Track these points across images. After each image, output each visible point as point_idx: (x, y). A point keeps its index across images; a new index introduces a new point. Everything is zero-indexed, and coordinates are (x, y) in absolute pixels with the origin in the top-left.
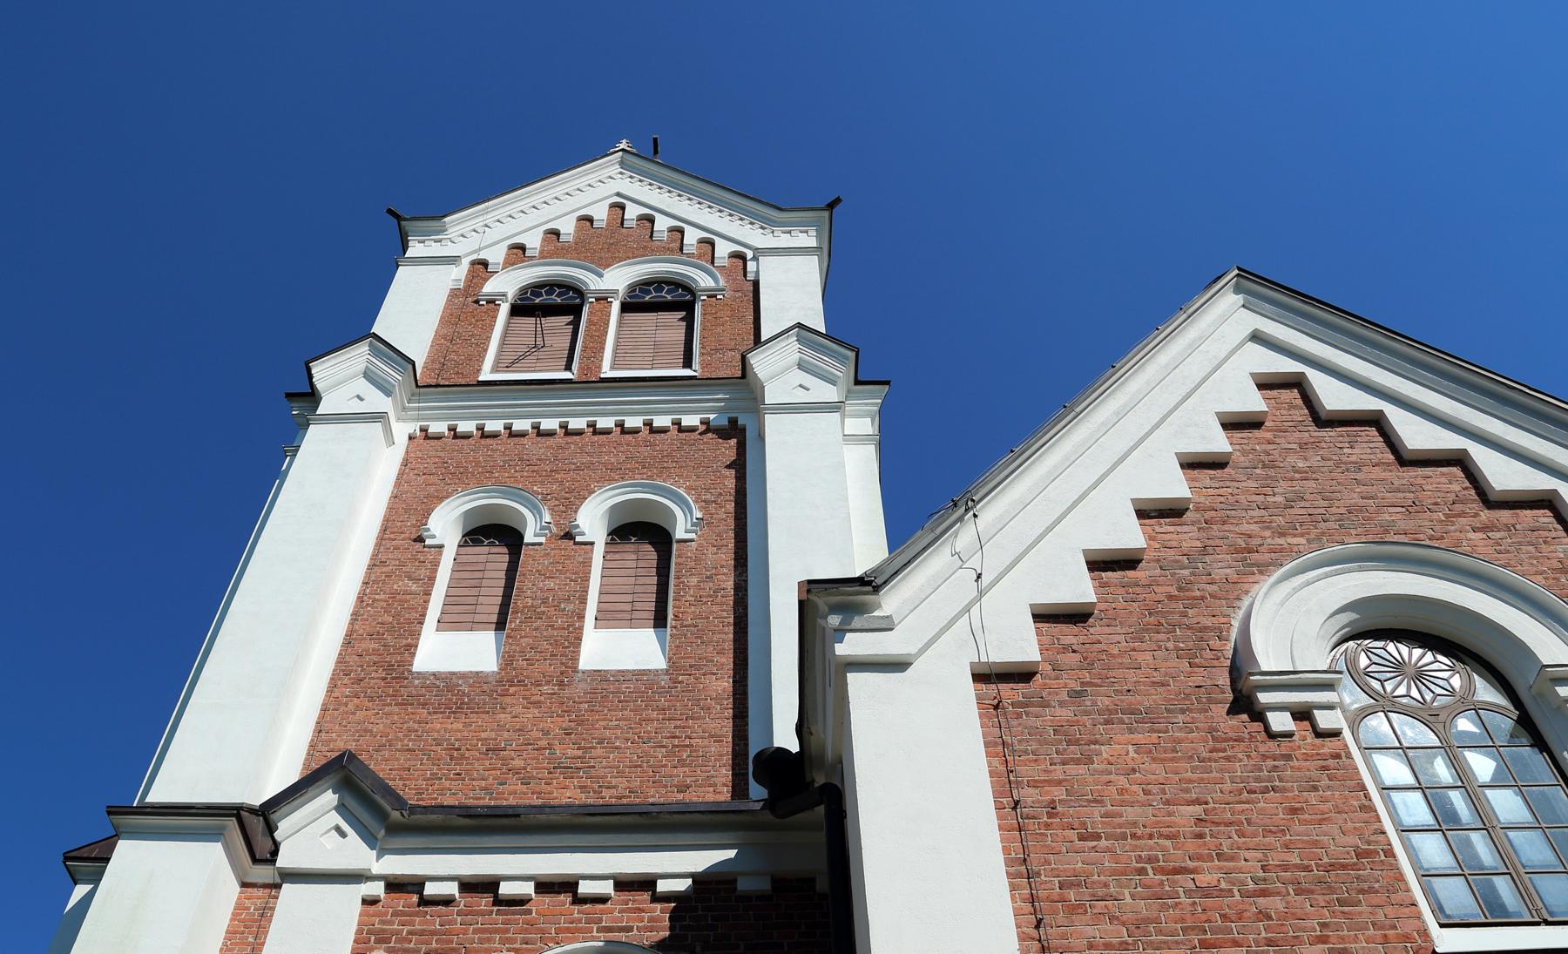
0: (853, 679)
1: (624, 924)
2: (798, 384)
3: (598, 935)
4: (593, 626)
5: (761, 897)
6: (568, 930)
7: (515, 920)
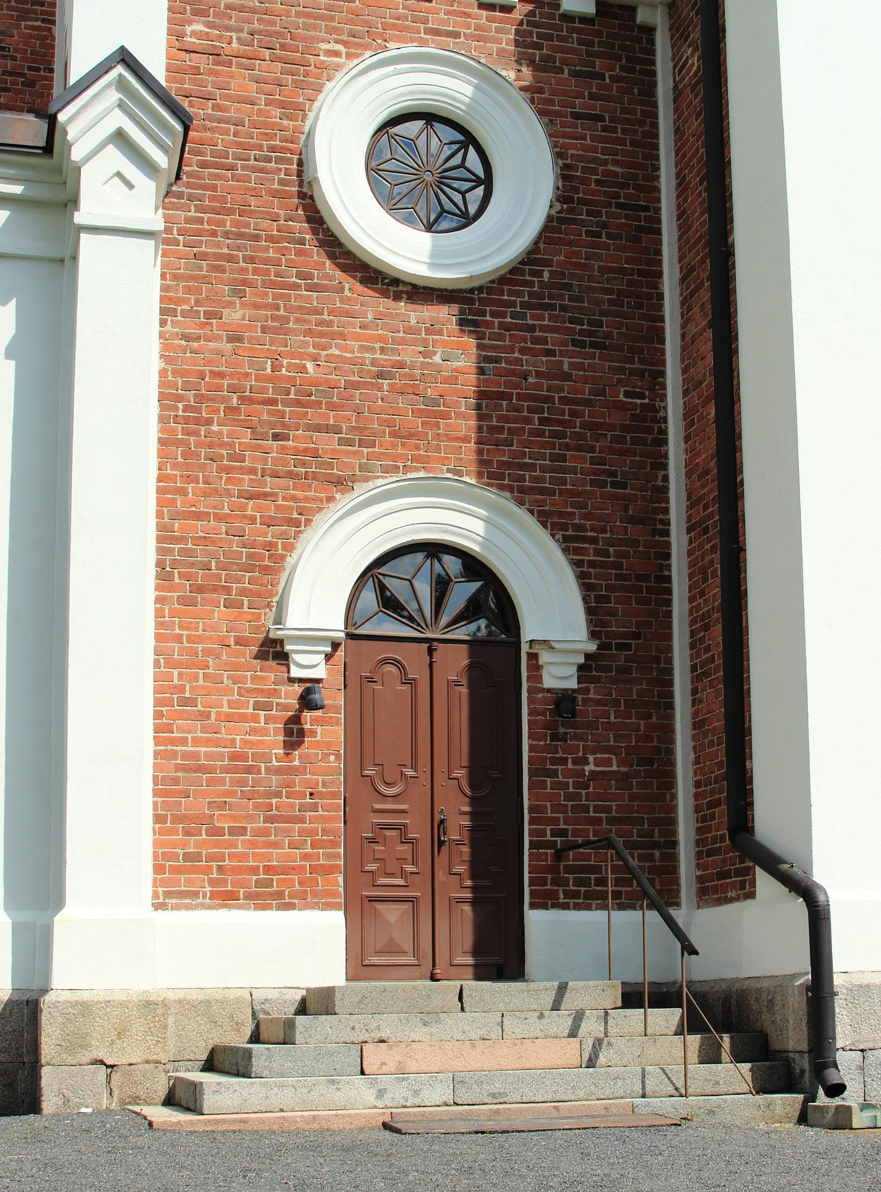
0: (84, 237)
1: (451, 28)
2: (115, 171)
3: (425, 36)
4: (624, 981)
5: (585, 19)
6: (394, 27)
7: (339, 7)
